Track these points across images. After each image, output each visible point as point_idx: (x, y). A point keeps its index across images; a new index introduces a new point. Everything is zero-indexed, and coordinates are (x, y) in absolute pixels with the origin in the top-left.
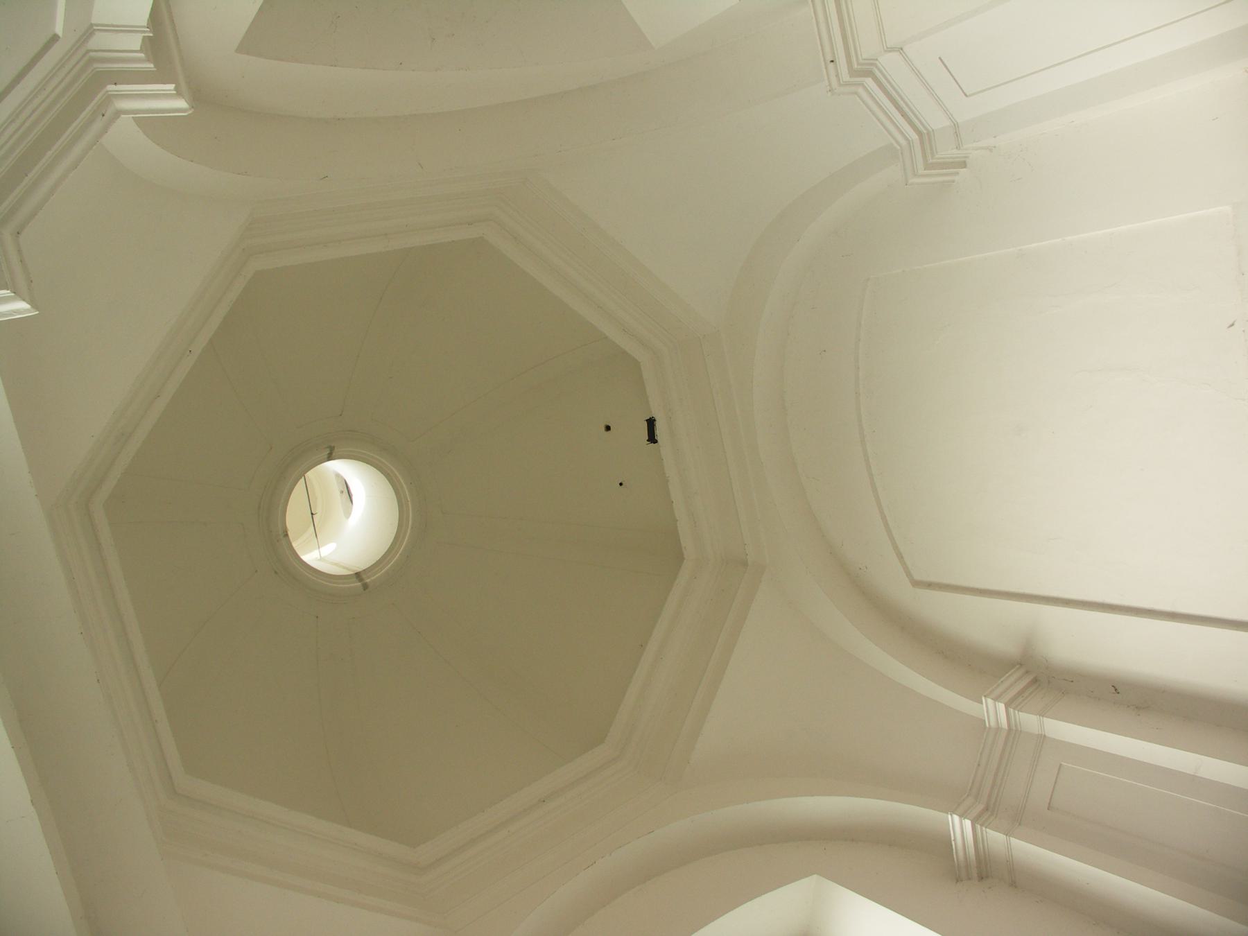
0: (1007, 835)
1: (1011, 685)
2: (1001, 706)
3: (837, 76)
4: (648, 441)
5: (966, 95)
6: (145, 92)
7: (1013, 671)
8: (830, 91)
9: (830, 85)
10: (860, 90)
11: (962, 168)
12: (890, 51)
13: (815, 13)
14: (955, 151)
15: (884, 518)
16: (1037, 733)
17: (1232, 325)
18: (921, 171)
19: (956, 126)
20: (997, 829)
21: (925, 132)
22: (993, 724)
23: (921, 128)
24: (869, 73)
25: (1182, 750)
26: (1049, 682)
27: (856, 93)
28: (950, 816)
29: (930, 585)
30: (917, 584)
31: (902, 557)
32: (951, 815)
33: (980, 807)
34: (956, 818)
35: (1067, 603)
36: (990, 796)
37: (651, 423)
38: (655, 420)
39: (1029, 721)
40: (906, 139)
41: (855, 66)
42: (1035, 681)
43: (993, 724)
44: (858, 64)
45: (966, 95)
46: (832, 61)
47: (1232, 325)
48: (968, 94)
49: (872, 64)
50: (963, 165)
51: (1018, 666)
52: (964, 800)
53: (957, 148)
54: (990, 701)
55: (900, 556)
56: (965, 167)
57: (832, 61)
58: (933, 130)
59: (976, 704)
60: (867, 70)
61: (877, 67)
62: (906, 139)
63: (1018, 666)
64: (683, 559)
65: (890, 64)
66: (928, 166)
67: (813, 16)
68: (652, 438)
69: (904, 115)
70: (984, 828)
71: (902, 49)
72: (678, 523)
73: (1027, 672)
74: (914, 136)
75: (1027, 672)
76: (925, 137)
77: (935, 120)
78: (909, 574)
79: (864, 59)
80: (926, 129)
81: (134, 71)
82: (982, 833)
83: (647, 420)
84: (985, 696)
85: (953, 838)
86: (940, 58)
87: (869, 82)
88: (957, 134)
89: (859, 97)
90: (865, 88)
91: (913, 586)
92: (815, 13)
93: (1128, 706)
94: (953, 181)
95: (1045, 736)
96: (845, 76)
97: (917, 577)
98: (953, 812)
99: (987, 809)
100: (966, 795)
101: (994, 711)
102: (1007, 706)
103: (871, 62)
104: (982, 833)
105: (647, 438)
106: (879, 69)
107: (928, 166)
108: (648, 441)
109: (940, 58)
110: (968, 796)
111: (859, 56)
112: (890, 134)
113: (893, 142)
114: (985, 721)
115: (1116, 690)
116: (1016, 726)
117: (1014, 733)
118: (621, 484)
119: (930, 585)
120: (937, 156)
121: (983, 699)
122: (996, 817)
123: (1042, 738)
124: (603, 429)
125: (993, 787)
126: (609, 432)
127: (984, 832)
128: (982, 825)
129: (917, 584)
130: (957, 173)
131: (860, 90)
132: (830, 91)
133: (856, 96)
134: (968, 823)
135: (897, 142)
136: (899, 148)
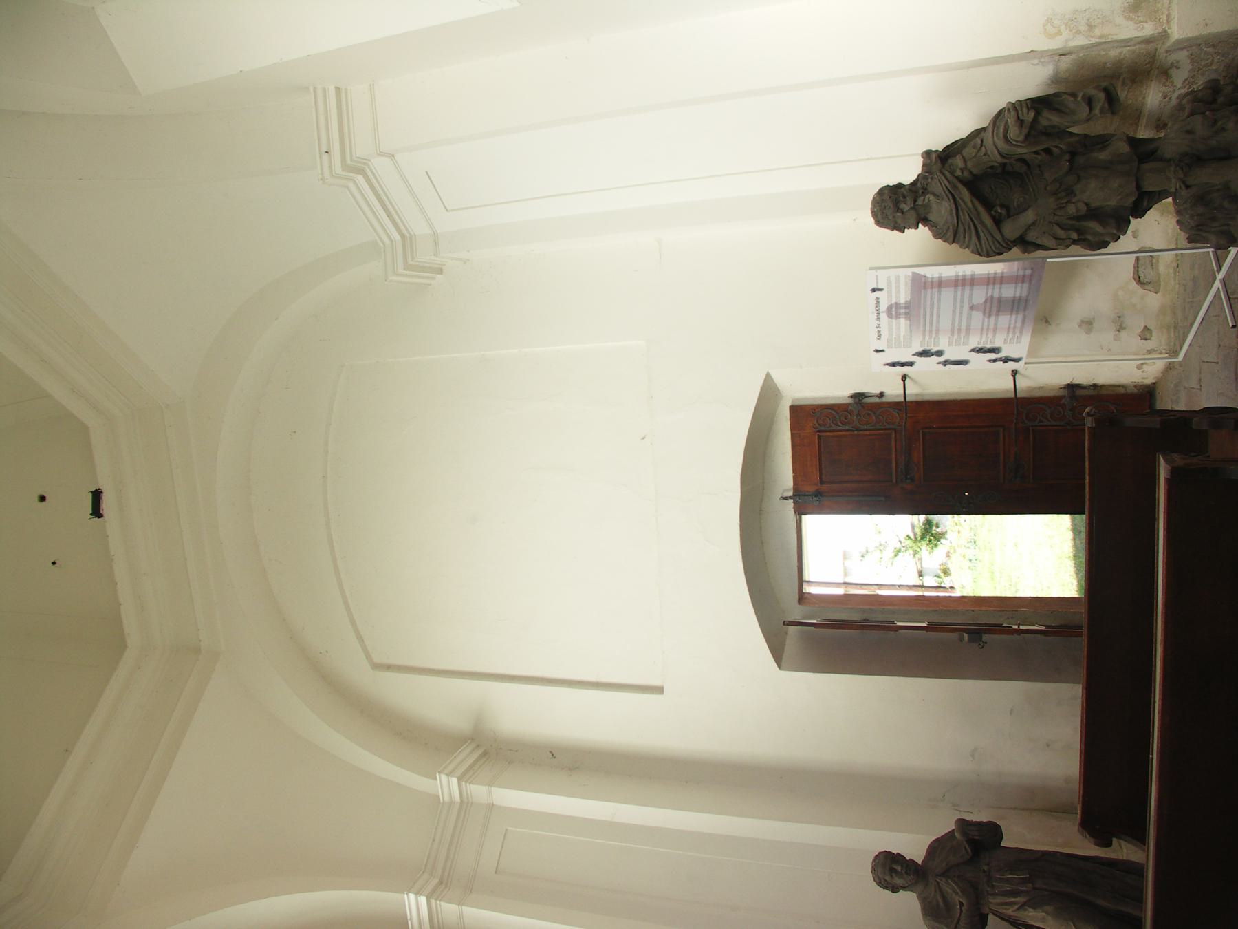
0: (459, 905)
1: (462, 762)
2: (454, 781)
3: (330, 167)
4: (91, 514)
5: (447, 210)
6: (422, 274)
7: (465, 746)
8: (321, 179)
9: (322, 174)
10: (351, 185)
11: (438, 274)
12: (383, 156)
13: (316, 102)
14: (433, 258)
15: (346, 602)
16: (486, 802)
17: (644, 438)
18: (401, 271)
19: (435, 235)
20: (450, 901)
21: (408, 235)
22: (447, 798)
23: (405, 232)
24: (361, 171)
25: (621, 803)
26: (497, 754)
27: (347, 187)
28: (406, 896)
29: (389, 667)
30: (377, 667)
31: (363, 641)
32: (407, 894)
33: (436, 881)
34: (412, 896)
35: (512, 680)
36: (443, 872)
37: (97, 495)
38: (102, 492)
39: (478, 791)
40: (390, 239)
41: (349, 162)
42: (485, 754)
43: (447, 798)
44: (351, 160)
45: (447, 210)
46: (327, 152)
47: (644, 438)
48: (448, 208)
49: (365, 164)
50: (440, 271)
51: (469, 741)
52: (420, 877)
53: (434, 255)
54: (444, 777)
55: (360, 639)
56: (441, 274)
57: (327, 152)
58: (415, 235)
59: (430, 781)
60: (359, 168)
61: (369, 167)
62: (390, 239)
63: (469, 741)
64: (126, 647)
65: (381, 166)
66: (407, 267)
67: (314, 105)
68: (97, 512)
69: (389, 215)
70: (438, 902)
71: (393, 156)
72: (122, 607)
73: (478, 746)
74: (397, 237)
75: (478, 746)
76: (408, 240)
77: (418, 228)
78: (368, 657)
79: (358, 158)
80: (409, 232)
81: (1155, 461)
82: (436, 907)
83: (92, 492)
84: (439, 772)
85: (409, 918)
86: (427, 173)
87: (360, 179)
88: (436, 243)
89: (349, 191)
90: (355, 183)
91: (372, 668)
92: (316, 102)
93: (563, 769)
94: (430, 285)
95: (493, 805)
96: (338, 169)
97: (377, 659)
98: (409, 891)
99: (441, 883)
100: (421, 872)
101: (447, 786)
102: (459, 780)
103: (364, 161)
104: (436, 907)
105: (91, 512)
106: (369, 167)
107: (407, 267)
108: (91, 514)
109: (427, 173)
110: (423, 872)
111: (354, 154)
112: (375, 231)
113: (377, 238)
114: (439, 797)
115: (553, 755)
116: (468, 798)
117: (466, 805)
118: (54, 563)
119: (389, 667)
120: (416, 259)
121: (437, 775)
122: (449, 890)
123: (491, 806)
124: (37, 499)
125: (446, 861)
126: (44, 503)
127: (439, 906)
128: (436, 900)
129: (377, 667)
130: (433, 278)
131: (351, 185)
132: (321, 179)
133: (347, 191)
134: (423, 899)
135: (381, 240)
136: (381, 245)
